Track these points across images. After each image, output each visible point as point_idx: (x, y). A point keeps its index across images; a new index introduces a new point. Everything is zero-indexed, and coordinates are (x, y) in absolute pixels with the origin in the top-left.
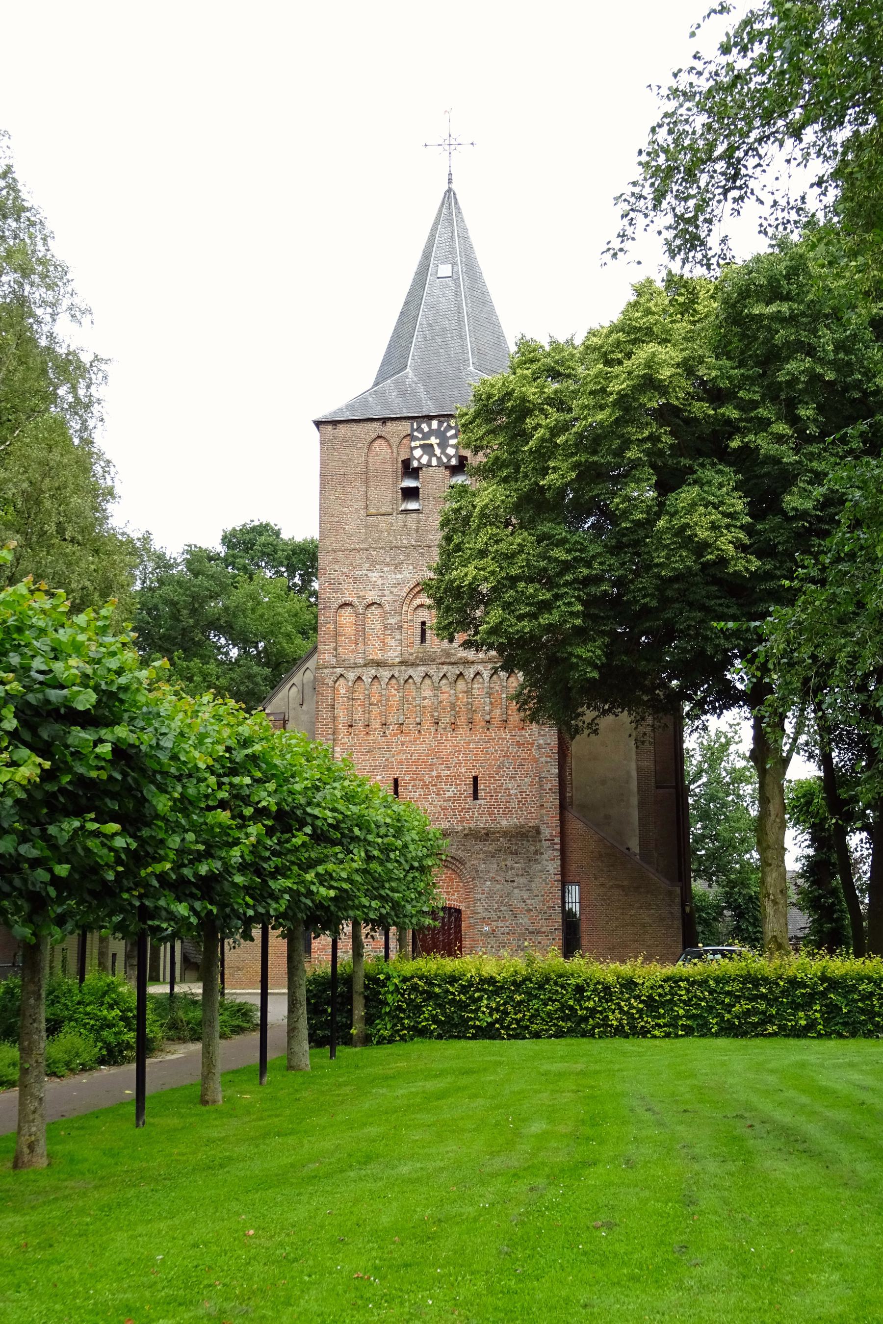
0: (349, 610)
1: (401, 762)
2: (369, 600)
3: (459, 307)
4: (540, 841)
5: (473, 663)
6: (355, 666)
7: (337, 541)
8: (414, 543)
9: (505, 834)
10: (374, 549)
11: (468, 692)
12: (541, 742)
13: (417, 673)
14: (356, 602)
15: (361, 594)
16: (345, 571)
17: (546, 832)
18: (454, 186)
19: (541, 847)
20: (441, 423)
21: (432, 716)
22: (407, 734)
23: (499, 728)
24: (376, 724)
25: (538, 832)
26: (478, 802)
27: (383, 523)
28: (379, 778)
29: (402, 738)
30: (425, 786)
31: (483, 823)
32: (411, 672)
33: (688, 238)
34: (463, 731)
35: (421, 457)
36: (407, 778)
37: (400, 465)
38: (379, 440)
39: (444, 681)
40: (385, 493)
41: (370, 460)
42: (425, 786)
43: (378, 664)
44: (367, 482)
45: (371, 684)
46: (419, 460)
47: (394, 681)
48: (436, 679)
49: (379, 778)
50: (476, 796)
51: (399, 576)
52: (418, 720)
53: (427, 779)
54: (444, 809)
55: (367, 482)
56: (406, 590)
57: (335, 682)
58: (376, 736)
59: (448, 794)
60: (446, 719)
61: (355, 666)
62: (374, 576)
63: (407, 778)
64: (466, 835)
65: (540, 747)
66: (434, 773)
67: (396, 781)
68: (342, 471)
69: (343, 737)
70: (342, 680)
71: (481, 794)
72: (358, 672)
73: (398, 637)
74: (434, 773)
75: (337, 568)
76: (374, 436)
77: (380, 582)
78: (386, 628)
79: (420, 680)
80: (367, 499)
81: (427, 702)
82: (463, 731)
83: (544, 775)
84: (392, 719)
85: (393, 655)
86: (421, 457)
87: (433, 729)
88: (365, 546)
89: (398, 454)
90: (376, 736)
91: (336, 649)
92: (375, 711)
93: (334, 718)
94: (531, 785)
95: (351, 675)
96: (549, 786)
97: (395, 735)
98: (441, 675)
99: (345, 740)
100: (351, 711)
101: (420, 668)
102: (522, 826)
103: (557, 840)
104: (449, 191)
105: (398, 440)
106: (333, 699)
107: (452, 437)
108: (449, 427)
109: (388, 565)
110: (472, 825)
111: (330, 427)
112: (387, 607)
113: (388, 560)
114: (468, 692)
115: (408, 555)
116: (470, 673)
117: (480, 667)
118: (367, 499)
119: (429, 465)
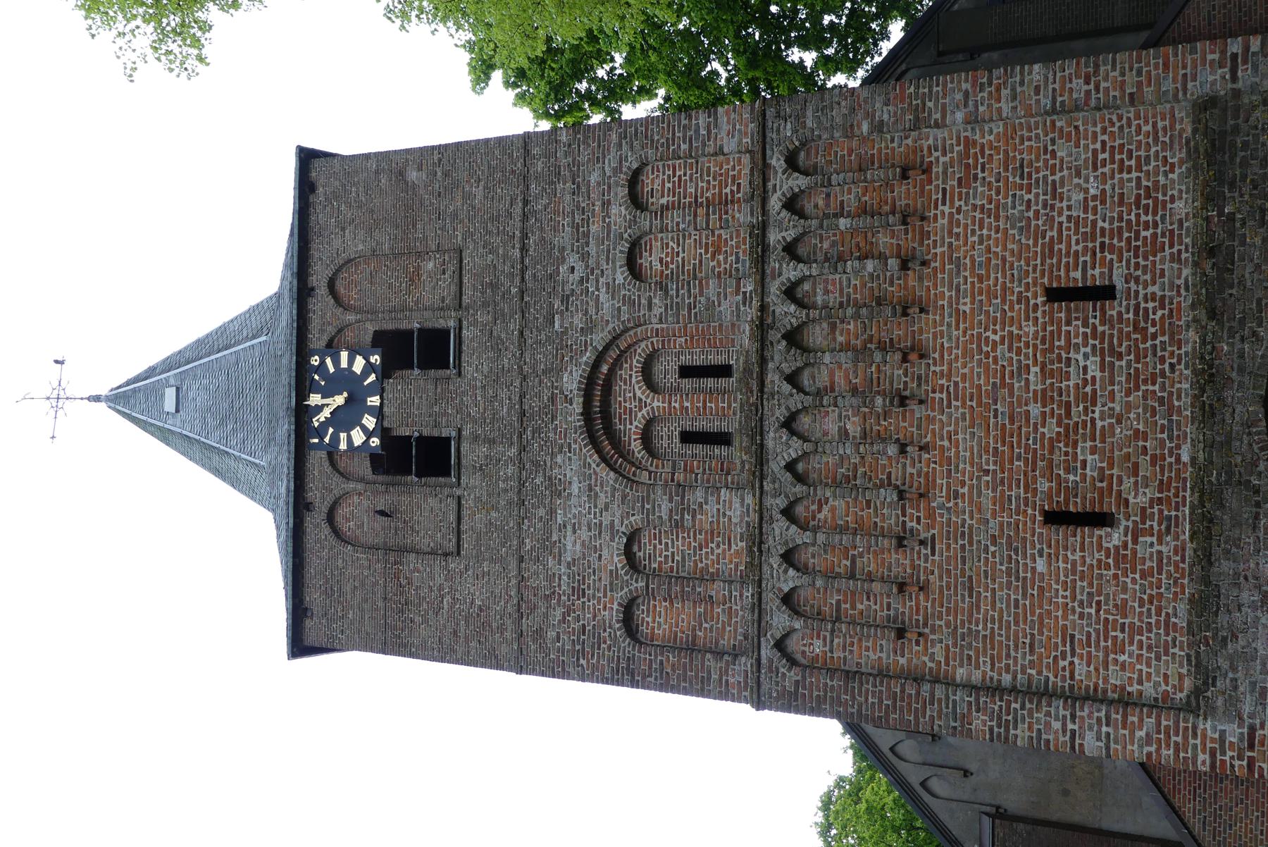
0: (641, 614)
1: (1003, 503)
2: (619, 561)
3: (238, 343)
4: (1237, 94)
5: (763, 308)
6: (758, 606)
7: (501, 629)
8: (513, 451)
9: (1211, 198)
10: (522, 543)
11: (832, 317)
12: (959, 116)
13: (781, 448)
14: (621, 595)
15: (605, 581)
16: (559, 612)
17: (1211, 79)
18: (104, 391)
19: (1254, 88)
20: (314, 388)
21: (886, 415)
22: (930, 482)
23: (924, 235)
24: (899, 563)
25: (1206, 105)
26: (1119, 284)
27: (475, 520)
28: (1041, 565)
29: (939, 499)
30: (1069, 435)
31: (1177, 273)
32: (776, 466)
33: (536, 126)
34: (928, 329)
35: (364, 429)
36: (1043, 485)
37: (380, 478)
38: (339, 519)
39: (806, 381)
40: (425, 505)
41: (370, 540)
42: (1069, 435)
43: (757, 541)
44: (403, 550)
45: (802, 569)
46: (369, 434)
47: (800, 510)
48: (797, 401)
49: (1041, 565)
50: (1105, 293)
51: (575, 489)
52: (892, 450)
53: (1051, 429)
54: (1135, 380)
55: (403, 550)
56: (604, 472)
57: (793, 662)
58: (931, 565)
59: (1094, 371)
60: (896, 374)
61: (758, 606)
62: (572, 546)
63: (1043, 485)
64: (1212, 314)
65: (973, 120)
66: (1035, 410)
67: (1055, 518)
68: (380, 604)
69: (930, 654)
70: (794, 645)
71: (1096, 275)
72: (772, 601)
73: (699, 495)
74: (1035, 410)
75: (551, 634)
76: (326, 530)
77: (584, 534)
78: (679, 525)
79: (796, 443)
80: (433, 553)
81: (853, 427)
82: (928, 329)
83: (1046, 102)
84: (890, 518)
85: (736, 508)
86: (364, 429)
87: (919, 411)
88: (513, 564)
89: (362, 480)
90: (931, 565)
91: (719, 654)
92: (868, 563)
93: (882, 674)
94: (1075, 137)
95: (780, 620)
96: (1078, 84)
97: (931, 514)
98: (786, 388)
99: (938, 650)
100: (865, 623)
101: (770, 443)
102: (1192, 154)
103: (1235, 46)
104: (89, 399)
105: (337, 478)
106: (832, 672)
107: (336, 362)
108: (322, 367)
109: (552, 512)
110: (1186, 300)
111: (308, 623)
112: (636, 519)
113: (542, 512)
114: (832, 317)
115: (536, 464)
116: (787, 313)
117: (774, 288)
118: (433, 553)
119: (379, 413)
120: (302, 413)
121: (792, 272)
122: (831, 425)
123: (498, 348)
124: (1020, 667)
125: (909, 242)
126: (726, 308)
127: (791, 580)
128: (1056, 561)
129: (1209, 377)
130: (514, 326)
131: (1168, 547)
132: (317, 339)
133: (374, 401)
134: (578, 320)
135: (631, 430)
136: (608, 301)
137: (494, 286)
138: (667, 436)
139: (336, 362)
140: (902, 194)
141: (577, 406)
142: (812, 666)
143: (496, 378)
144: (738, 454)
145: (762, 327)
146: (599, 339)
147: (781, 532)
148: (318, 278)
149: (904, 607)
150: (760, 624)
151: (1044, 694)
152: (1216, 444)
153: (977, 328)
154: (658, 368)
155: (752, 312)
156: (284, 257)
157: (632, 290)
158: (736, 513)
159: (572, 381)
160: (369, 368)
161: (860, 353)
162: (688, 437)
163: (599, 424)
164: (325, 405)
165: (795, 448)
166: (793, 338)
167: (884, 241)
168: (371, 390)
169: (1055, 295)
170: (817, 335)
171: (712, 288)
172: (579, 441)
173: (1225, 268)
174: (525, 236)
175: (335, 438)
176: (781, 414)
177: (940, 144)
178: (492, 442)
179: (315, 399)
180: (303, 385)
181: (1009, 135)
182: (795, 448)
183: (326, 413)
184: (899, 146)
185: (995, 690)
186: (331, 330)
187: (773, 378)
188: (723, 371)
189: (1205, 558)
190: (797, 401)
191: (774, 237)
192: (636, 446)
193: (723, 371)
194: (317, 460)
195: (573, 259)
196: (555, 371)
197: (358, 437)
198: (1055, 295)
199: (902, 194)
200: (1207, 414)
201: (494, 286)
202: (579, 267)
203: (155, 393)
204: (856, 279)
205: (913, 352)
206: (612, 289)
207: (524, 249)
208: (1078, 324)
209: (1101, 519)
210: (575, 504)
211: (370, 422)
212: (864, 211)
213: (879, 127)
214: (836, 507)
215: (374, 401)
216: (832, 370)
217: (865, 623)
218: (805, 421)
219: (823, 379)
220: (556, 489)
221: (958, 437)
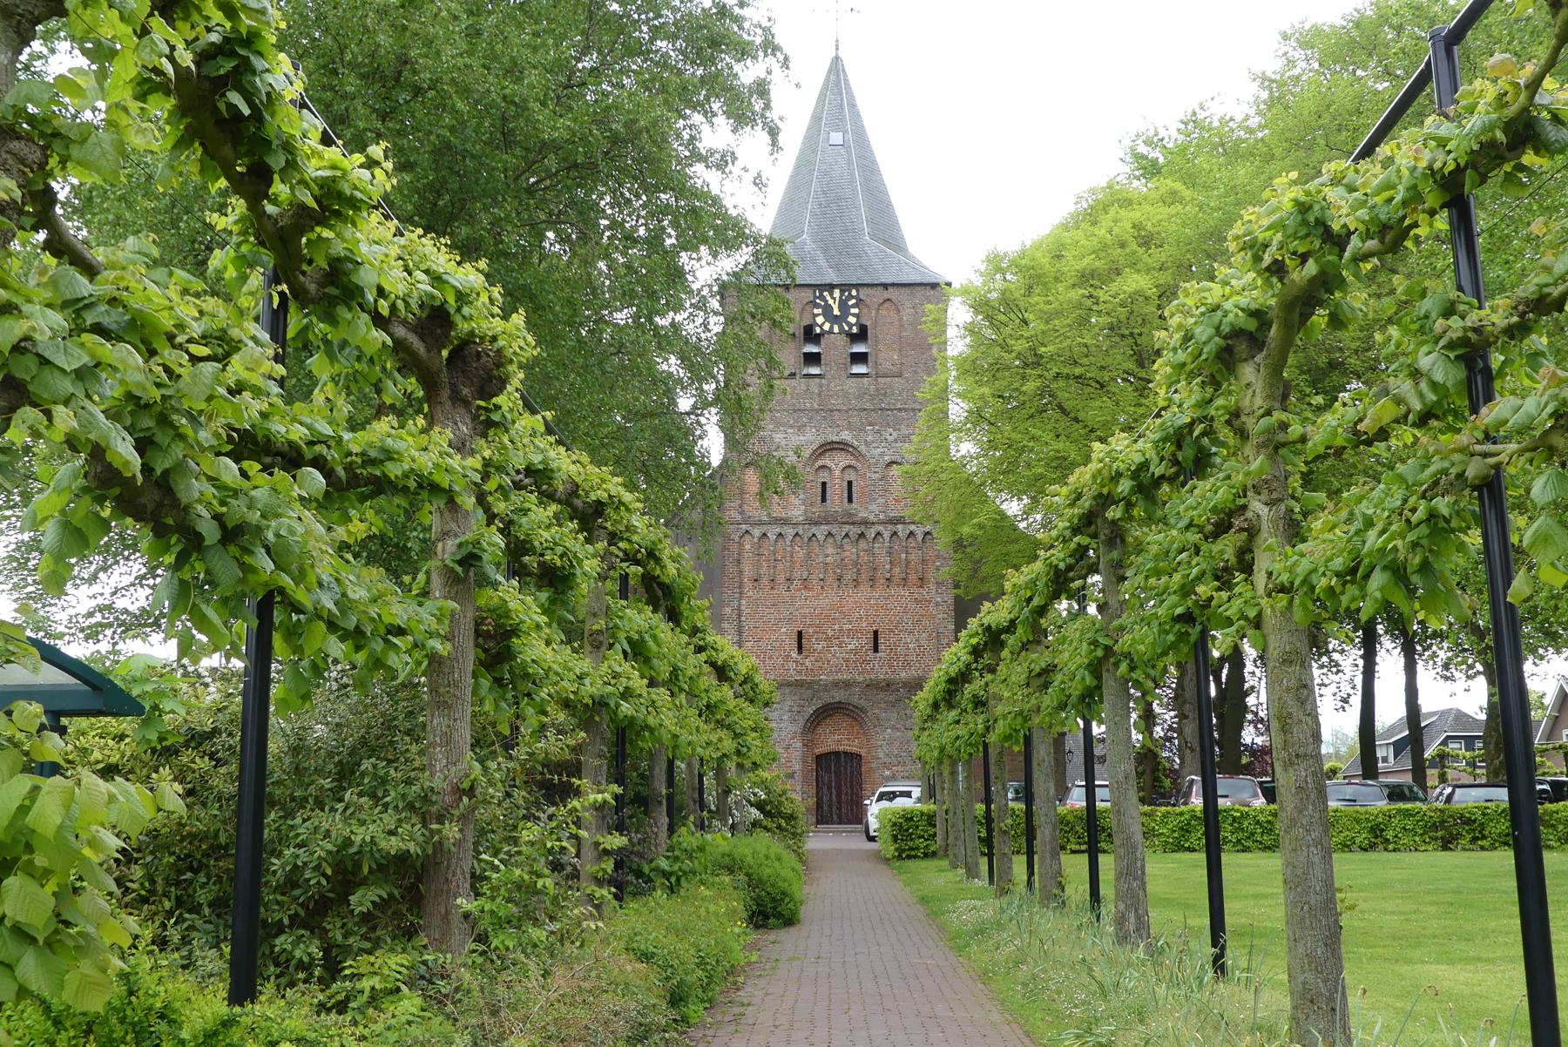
6: (761, 523)
11: (869, 551)
13: (821, 531)
24: (781, 578)
30: (828, 639)
31: (881, 673)
32: (814, 530)
34: (865, 587)
42: (828, 639)
43: (785, 522)
48: (838, 538)
50: (876, 650)
53: (830, 633)
54: (847, 660)
58: (781, 589)
60: (849, 576)
61: (761, 523)
65: (937, 604)
67: (800, 633)
72: (763, 529)
82: (865, 587)
84: (796, 575)
90: (781, 589)
92: (780, 566)
95: (757, 532)
100: (758, 566)
107: (853, 306)
109: (792, 427)
114: (869, 551)
116: (871, 533)
117: (881, 528)
119: (831, 332)
120: (831, 287)
121: (887, 535)
122: (830, 551)
123: (860, 397)
124: (748, 624)
125: (896, 580)
126: (873, 507)
127: (772, 537)
128: (786, 634)
129: (847, 685)
130: (868, 406)
131: (792, 672)
132: (864, 293)
133: (836, 329)
134: (870, 438)
135: (826, 461)
136: (878, 452)
137: (885, 395)
138: (824, 476)
139: (853, 306)
140: (913, 577)
141: (835, 439)
142: (741, 544)
143: (846, 396)
144: (818, 510)
145: (866, 523)
146: (863, 448)
147: (789, 532)
148: (892, 293)
149: (765, 581)
150: (754, 525)
151: (740, 633)
152: (825, 688)
153: (863, 606)
154: (851, 471)
155: (872, 518)
156: (926, 263)
157: (882, 464)
158: (796, 513)
159: (846, 436)
160: (850, 325)
161: (856, 564)
162: (824, 484)
163: (828, 447)
164: (833, 300)
165: (821, 537)
166: (862, 535)
167: (897, 570)
168: (841, 328)
169: (876, 633)
170: (863, 544)
171: (881, 501)
172: (820, 440)
173: (883, 689)
174: (905, 410)
175: (818, 306)
176: (834, 531)
177: (930, 592)
178: (820, 395)
179: (837, 293)
180: (844, 287)
181: (932, 616)
182: (821, 537)
183: (831, 302)
184: (930, 575)
185: (739, 616)
186: (868, 301)
187: (847, 528)
188: (850, 500)
189: (789, 685)
190: (838, 538)
191: (900, 527)
192: (820, 463)
193: (850, 500)
194: (807, 295)
195: (895, 435)
196: (850, 427)
197: (820, 320)
198: (876, 633)
199: (913, 577)
200: (836, 684)
201: (885, 395)
202: (890, 438)
203: (838, 125)
204: (884, 560)
205: (856, 583)
206: (882, 454)
207: (900, 410)
208: (866, 641)
209: (800, 648)
210: (797, 439)
211: (827, 327)
212: (908, 562)
213: (937, 569)
214: (800, 553)
215: (836, 329)
216: (850, 551)
217: (758, 566)
218: (831, 540)
219: (847, 547)
220: (801, 429)
221: (826, 600)
